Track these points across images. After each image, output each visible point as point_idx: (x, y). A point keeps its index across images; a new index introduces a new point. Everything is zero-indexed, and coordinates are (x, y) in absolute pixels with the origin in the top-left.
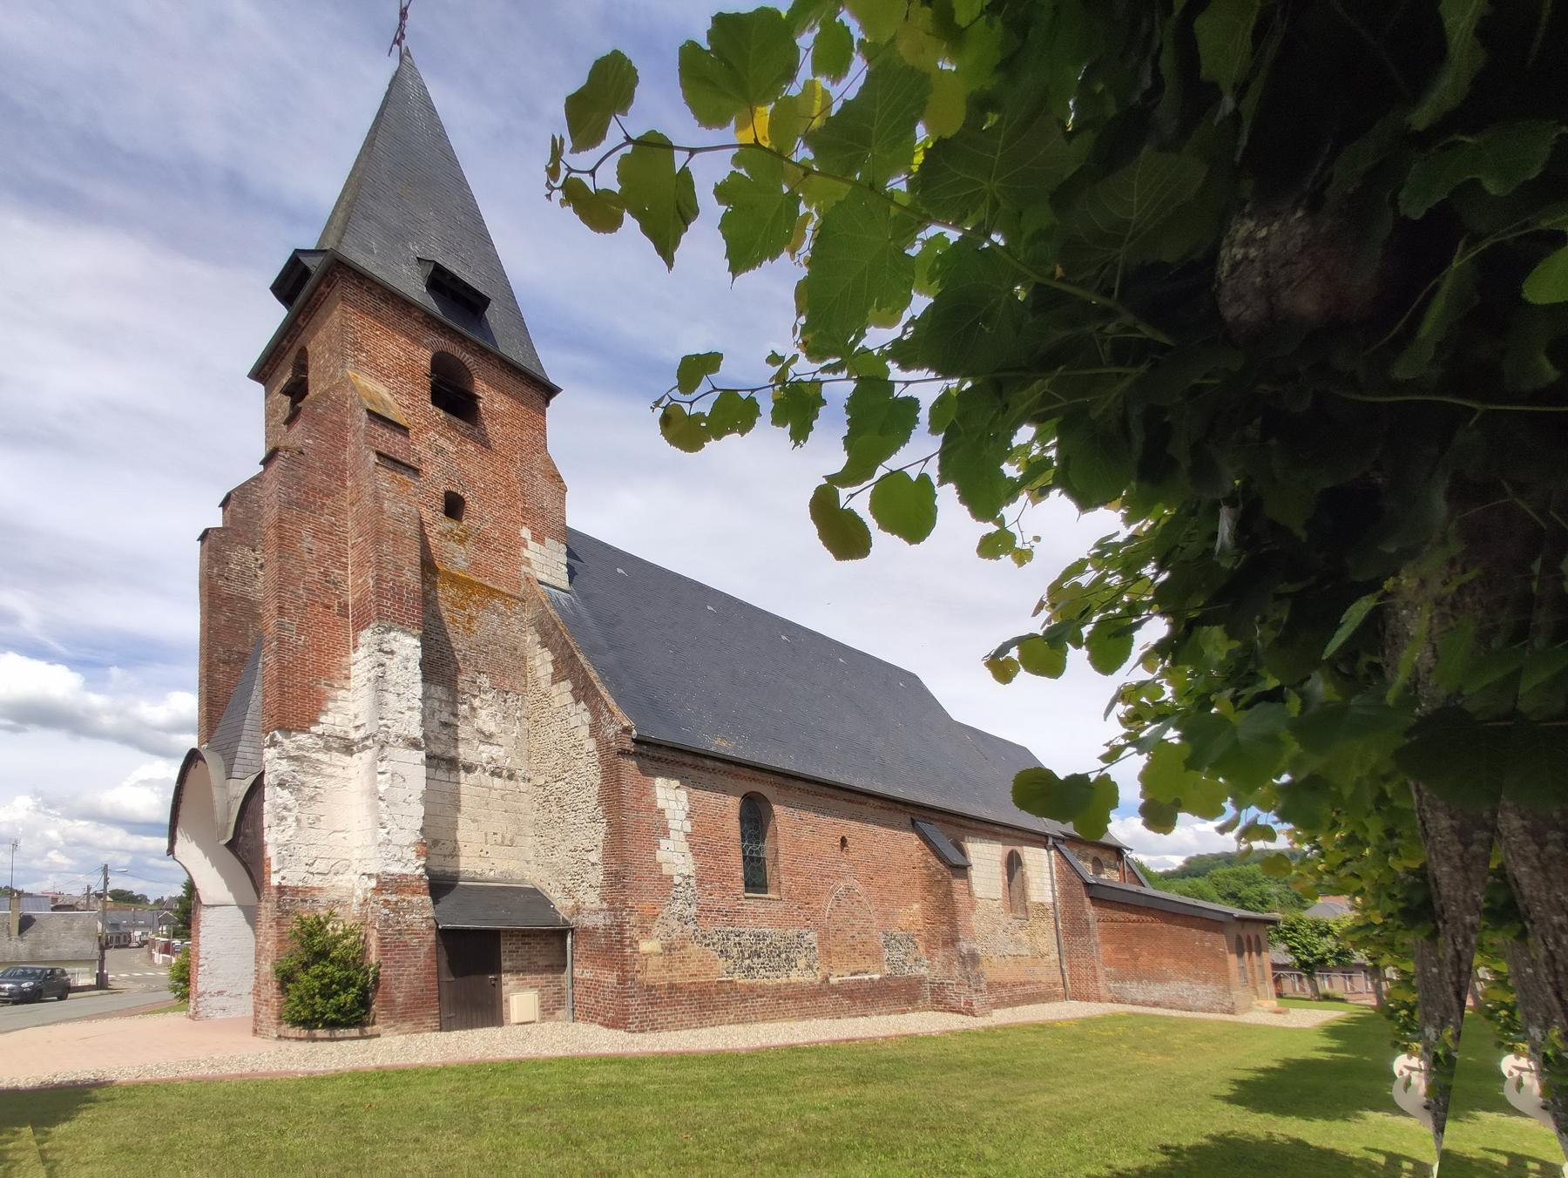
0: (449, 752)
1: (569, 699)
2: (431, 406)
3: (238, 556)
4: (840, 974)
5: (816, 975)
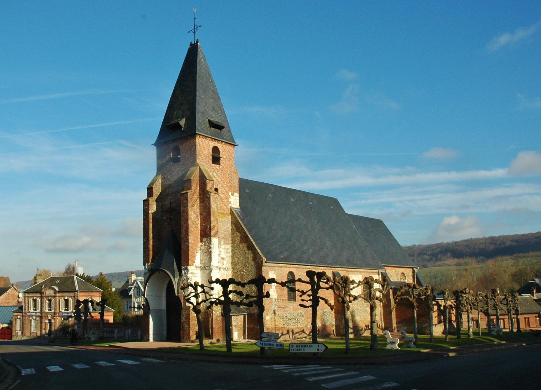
2: (212, 164)
5: (304, 325)
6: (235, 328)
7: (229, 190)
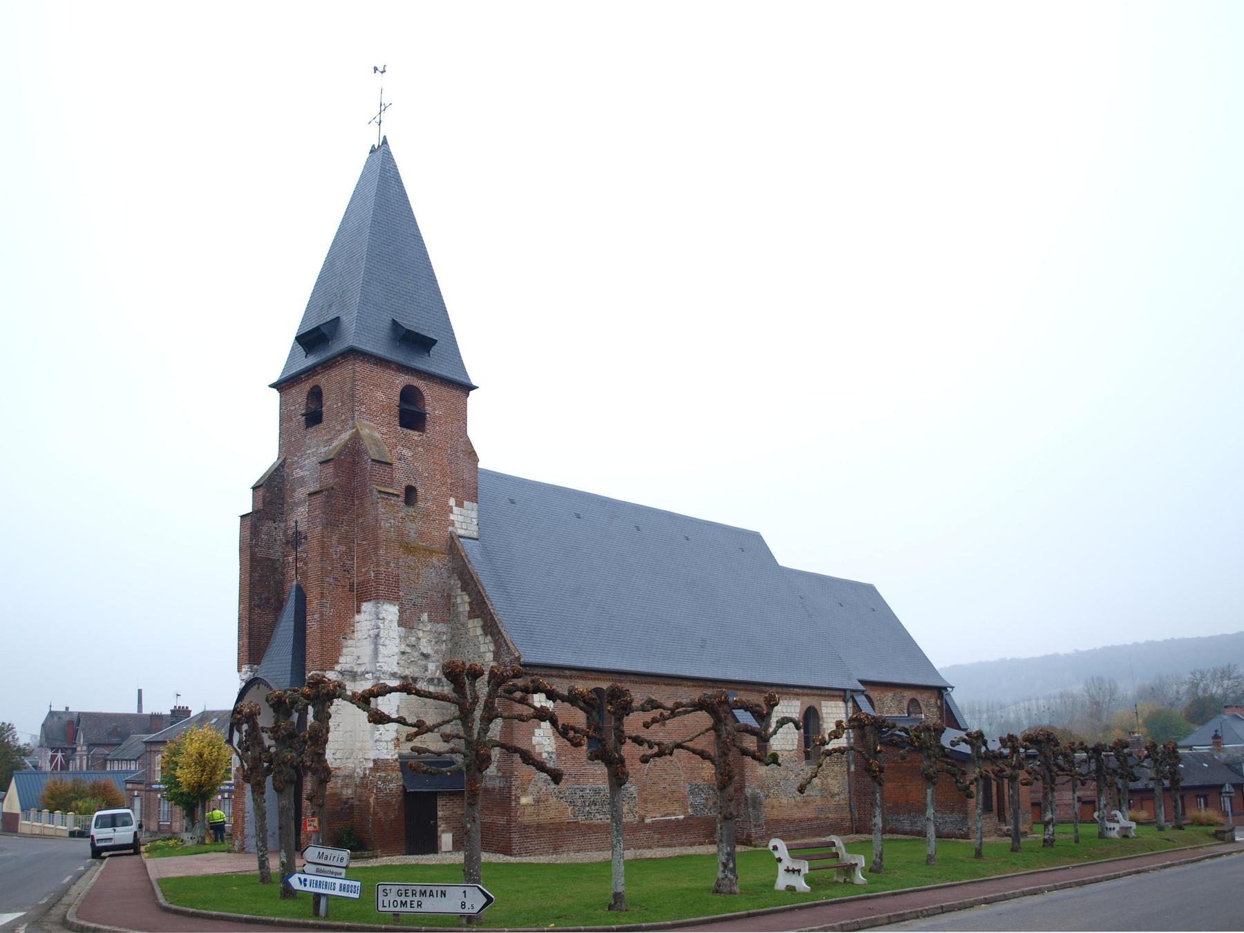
0: (404, 672)
1: (479, 631)
2: (399, 428)
3: (267, 526)
4: (654, 815)
5: (635, 817)
6: (446, 823)
7: (450, 493)
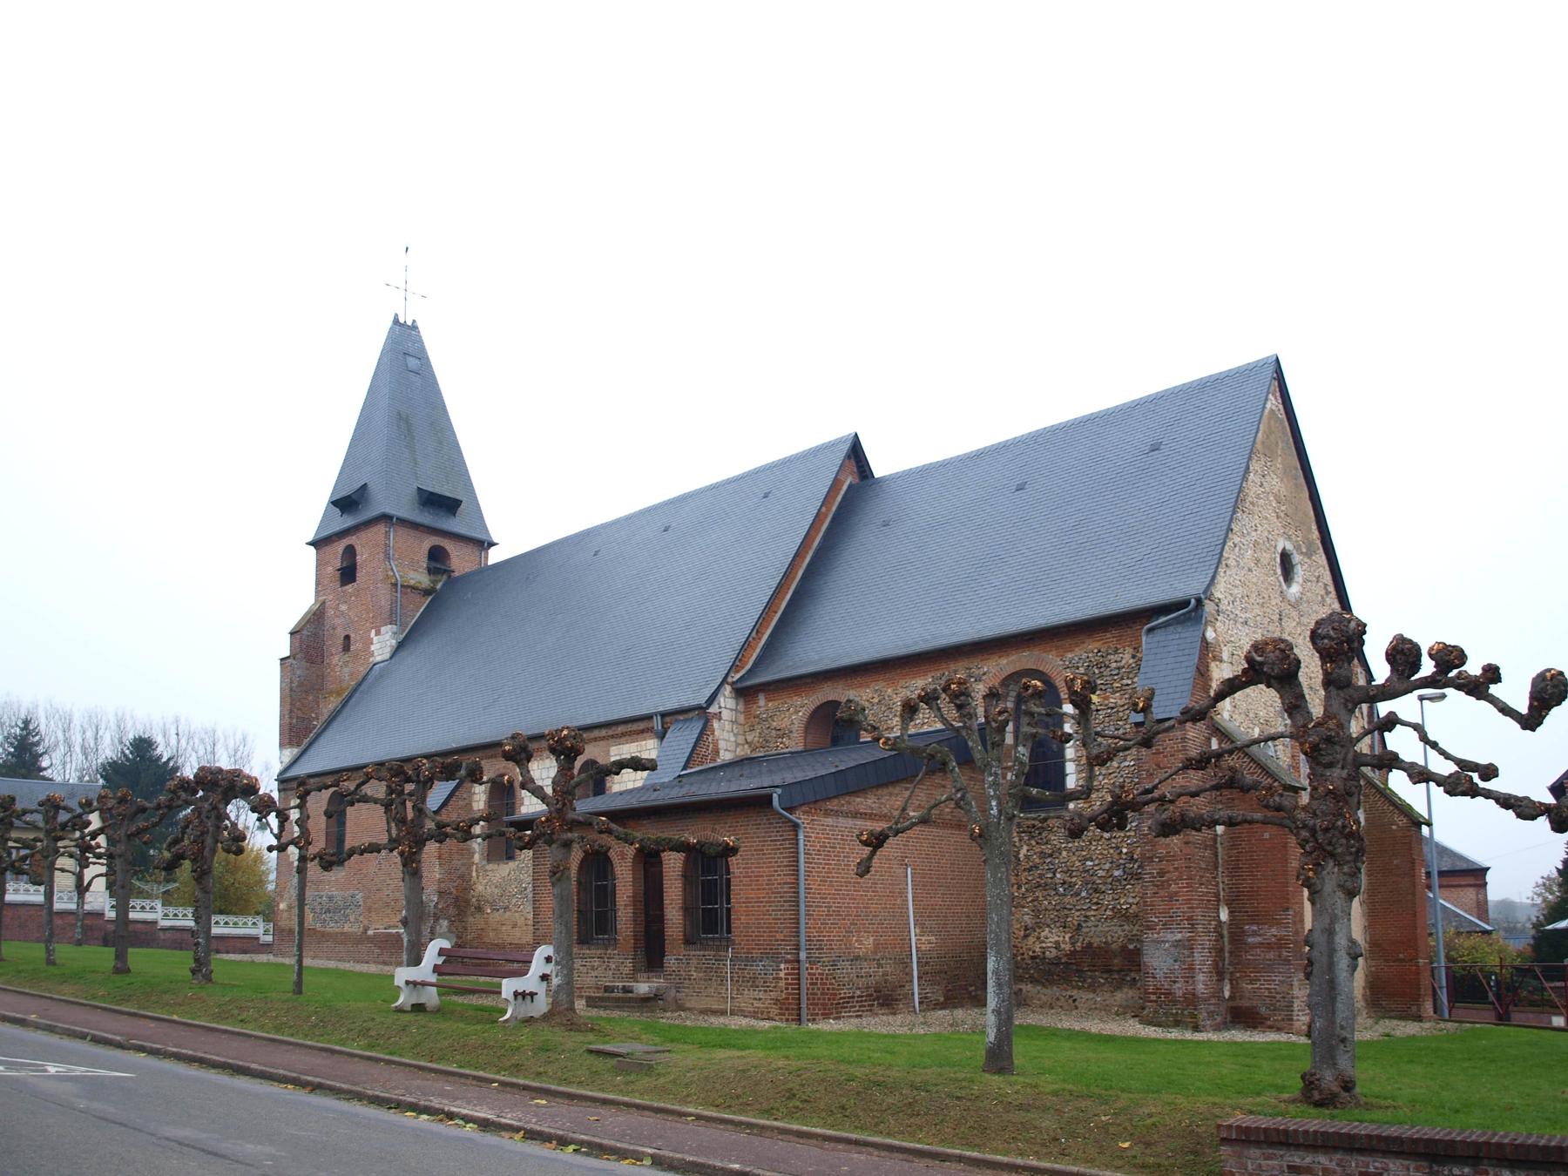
4: (377, 927)
